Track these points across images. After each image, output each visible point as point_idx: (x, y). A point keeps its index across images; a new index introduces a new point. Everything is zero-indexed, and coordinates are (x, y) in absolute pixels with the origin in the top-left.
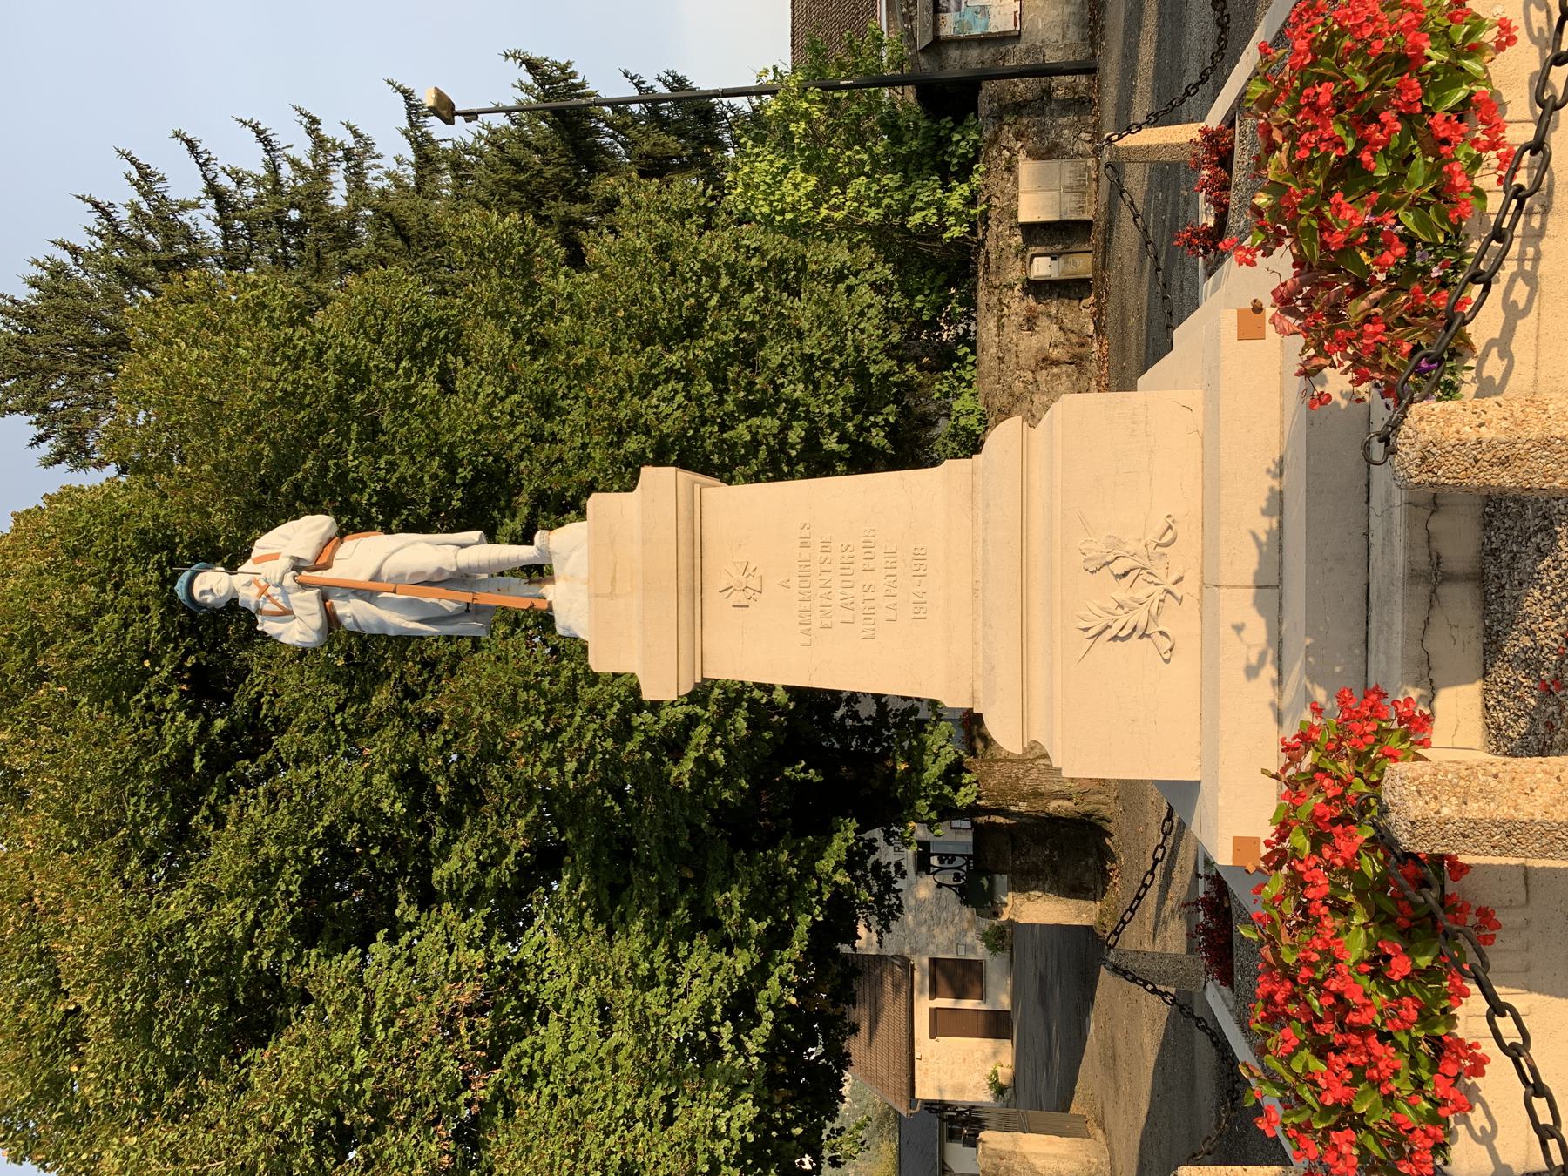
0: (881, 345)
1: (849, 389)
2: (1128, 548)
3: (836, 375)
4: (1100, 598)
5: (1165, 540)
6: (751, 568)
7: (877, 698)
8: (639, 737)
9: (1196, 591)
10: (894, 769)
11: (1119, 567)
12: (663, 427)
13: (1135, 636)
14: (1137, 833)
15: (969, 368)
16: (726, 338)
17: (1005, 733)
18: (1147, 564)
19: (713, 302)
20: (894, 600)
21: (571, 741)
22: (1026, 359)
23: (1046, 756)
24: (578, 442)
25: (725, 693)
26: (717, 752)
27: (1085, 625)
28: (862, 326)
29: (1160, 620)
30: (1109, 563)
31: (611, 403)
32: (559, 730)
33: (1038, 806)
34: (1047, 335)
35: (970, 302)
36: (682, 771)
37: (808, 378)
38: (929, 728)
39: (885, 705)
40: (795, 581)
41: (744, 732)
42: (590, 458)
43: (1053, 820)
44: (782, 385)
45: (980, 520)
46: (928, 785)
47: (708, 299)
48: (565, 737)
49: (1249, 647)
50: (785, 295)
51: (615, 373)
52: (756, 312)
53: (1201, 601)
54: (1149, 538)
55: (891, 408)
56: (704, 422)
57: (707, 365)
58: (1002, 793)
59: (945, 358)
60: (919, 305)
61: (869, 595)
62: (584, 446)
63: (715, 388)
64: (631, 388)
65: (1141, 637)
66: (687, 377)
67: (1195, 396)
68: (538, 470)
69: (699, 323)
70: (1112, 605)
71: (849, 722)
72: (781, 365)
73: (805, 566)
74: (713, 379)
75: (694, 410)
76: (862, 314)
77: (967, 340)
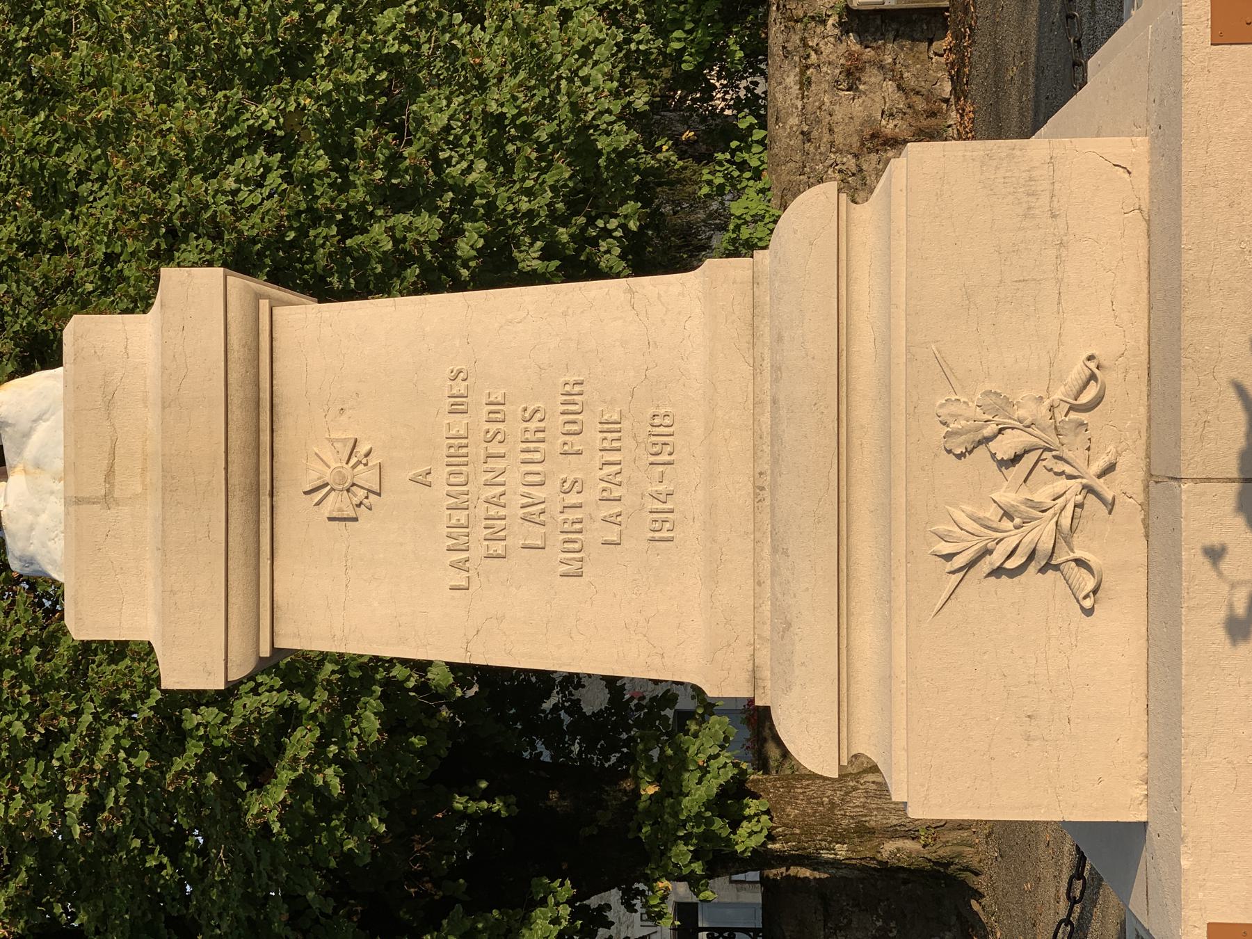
0: (617, 107)
1: (563, 171)
2: (1021, 413)
3: (541, 147)
4: (971, 503)
5: (1085, 398)
6: (362, 449)
7: (611, 682)
8: (195, 748)
9: (1138, 488)
10: (636, 794)
11: (1005, 446)
12: (243, 226)
13: (1033, 568)
14: (1022, 892)
15: (756, 149)
16: (352, 79)
17: (810, 743)
18: (1054, 440)
19: (331, 20)
20: (616, 508)
21: (76, 755)
22: (846, 135)
23: (874, 769)
24: (100, 252)
25: (344, 670)
26: (330, 772)
27: (947, 548)
28: (584, 72)
29: (1077, 540)
30: (987, 440)
31: (156, 185)
32: (54, 738)
33: (865, 850)
34: (879, 95)
35: (757, 52)
36: (267, 804)
37: (496, 156)
38: (693, 727)
39: (623, 687)
40: (440, 475)
41: (375, 737)
42: (121, 278)
43: (888, 871)
44: (448, 161)
45: (767, 364)
46: (689, 818)
47: (322, 16)
48: (65, 749)
49: (1233, 586)
50: (458, 17)
51: (163, 134)
52: (404, 39)
53: (1146, 506)
54: (1058, 395)
55: (630, 207)
56: (316, 218)
57: (321, 123)
58: (808, 831)
59: (721, 134)
60: (676, 45)
61: (573, 499)
62: (111, 258)
63: (335, 166)
64: (189, 160)
65: (1042, 570)
66: (282, 143)
67: (1134, 148)
68: (30, 298)
69: (306, 53)
70: (992, 513)
71: (566, 718)
72: (447, 129)
73: (458, 445)
74: (335, 151)
75: (298, 198)
76: (585, 53)
77: (753, 104)
